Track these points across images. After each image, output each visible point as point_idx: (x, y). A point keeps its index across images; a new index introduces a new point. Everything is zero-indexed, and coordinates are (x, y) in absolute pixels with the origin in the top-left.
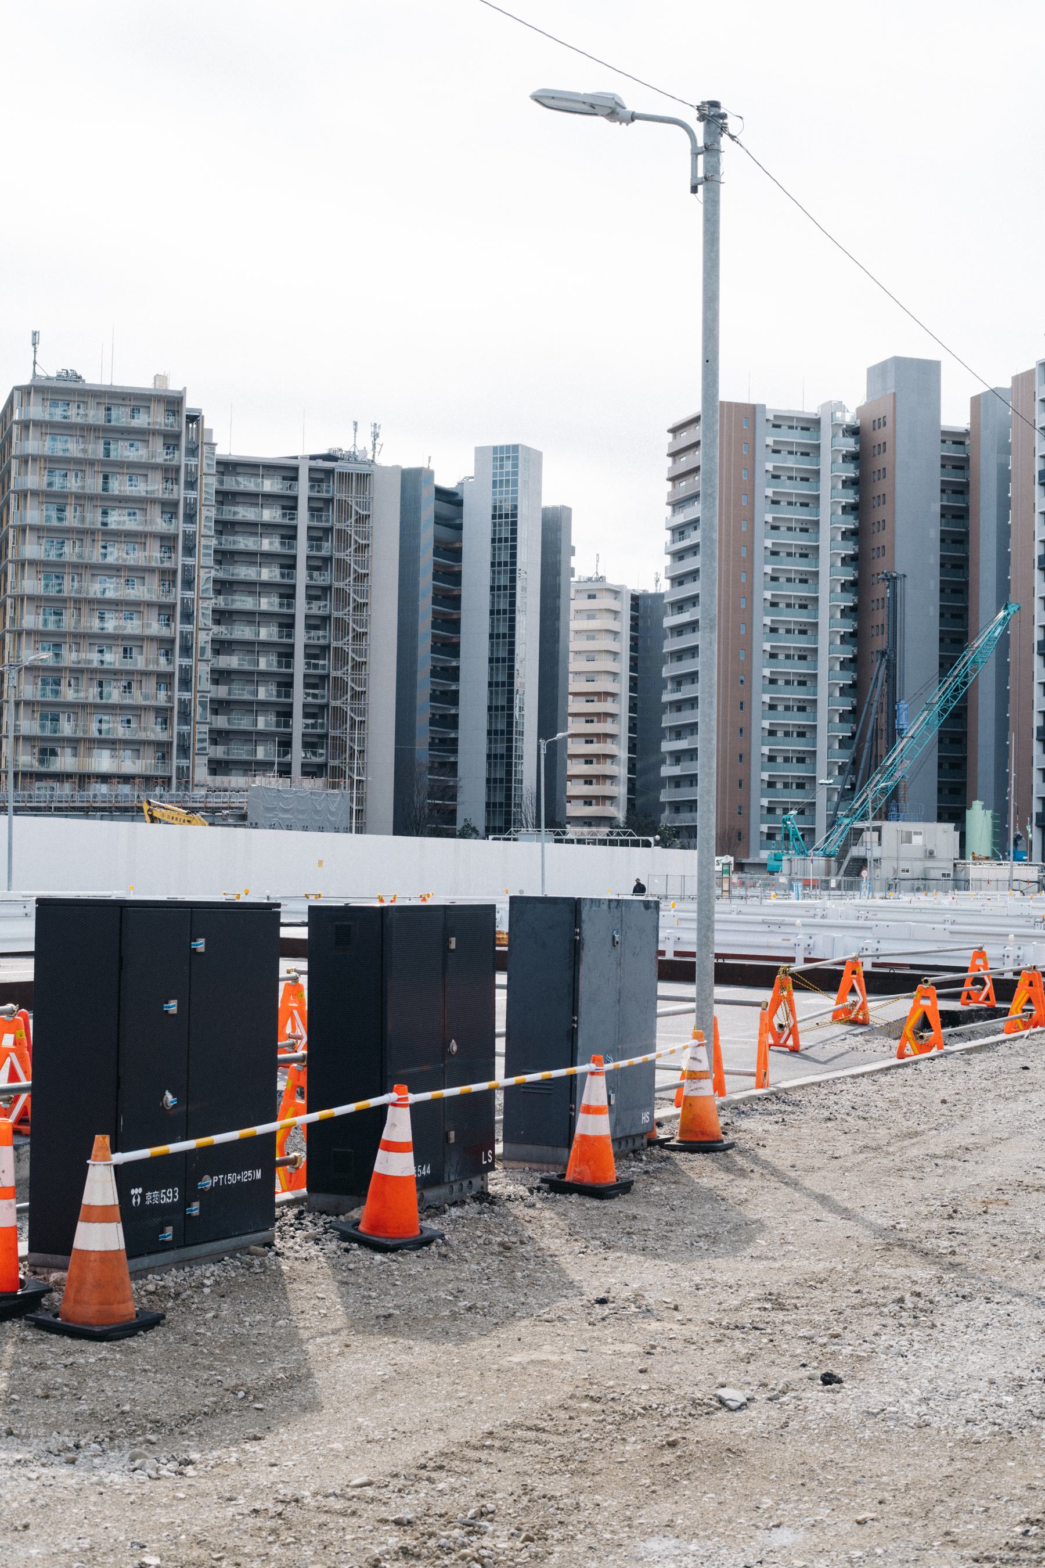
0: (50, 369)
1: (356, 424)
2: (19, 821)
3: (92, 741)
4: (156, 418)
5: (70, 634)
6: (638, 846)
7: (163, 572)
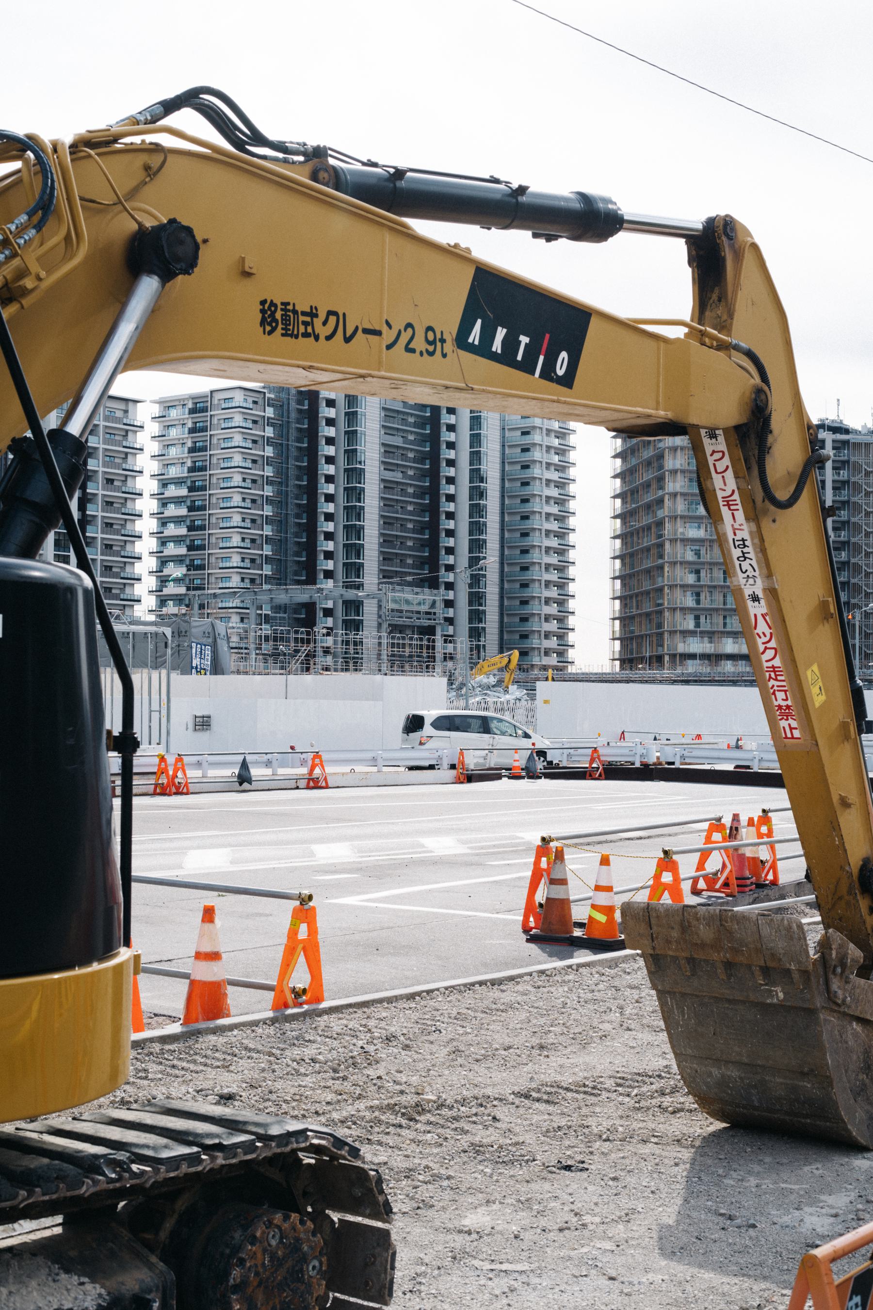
1: (838, 400)
5: (707, 563)
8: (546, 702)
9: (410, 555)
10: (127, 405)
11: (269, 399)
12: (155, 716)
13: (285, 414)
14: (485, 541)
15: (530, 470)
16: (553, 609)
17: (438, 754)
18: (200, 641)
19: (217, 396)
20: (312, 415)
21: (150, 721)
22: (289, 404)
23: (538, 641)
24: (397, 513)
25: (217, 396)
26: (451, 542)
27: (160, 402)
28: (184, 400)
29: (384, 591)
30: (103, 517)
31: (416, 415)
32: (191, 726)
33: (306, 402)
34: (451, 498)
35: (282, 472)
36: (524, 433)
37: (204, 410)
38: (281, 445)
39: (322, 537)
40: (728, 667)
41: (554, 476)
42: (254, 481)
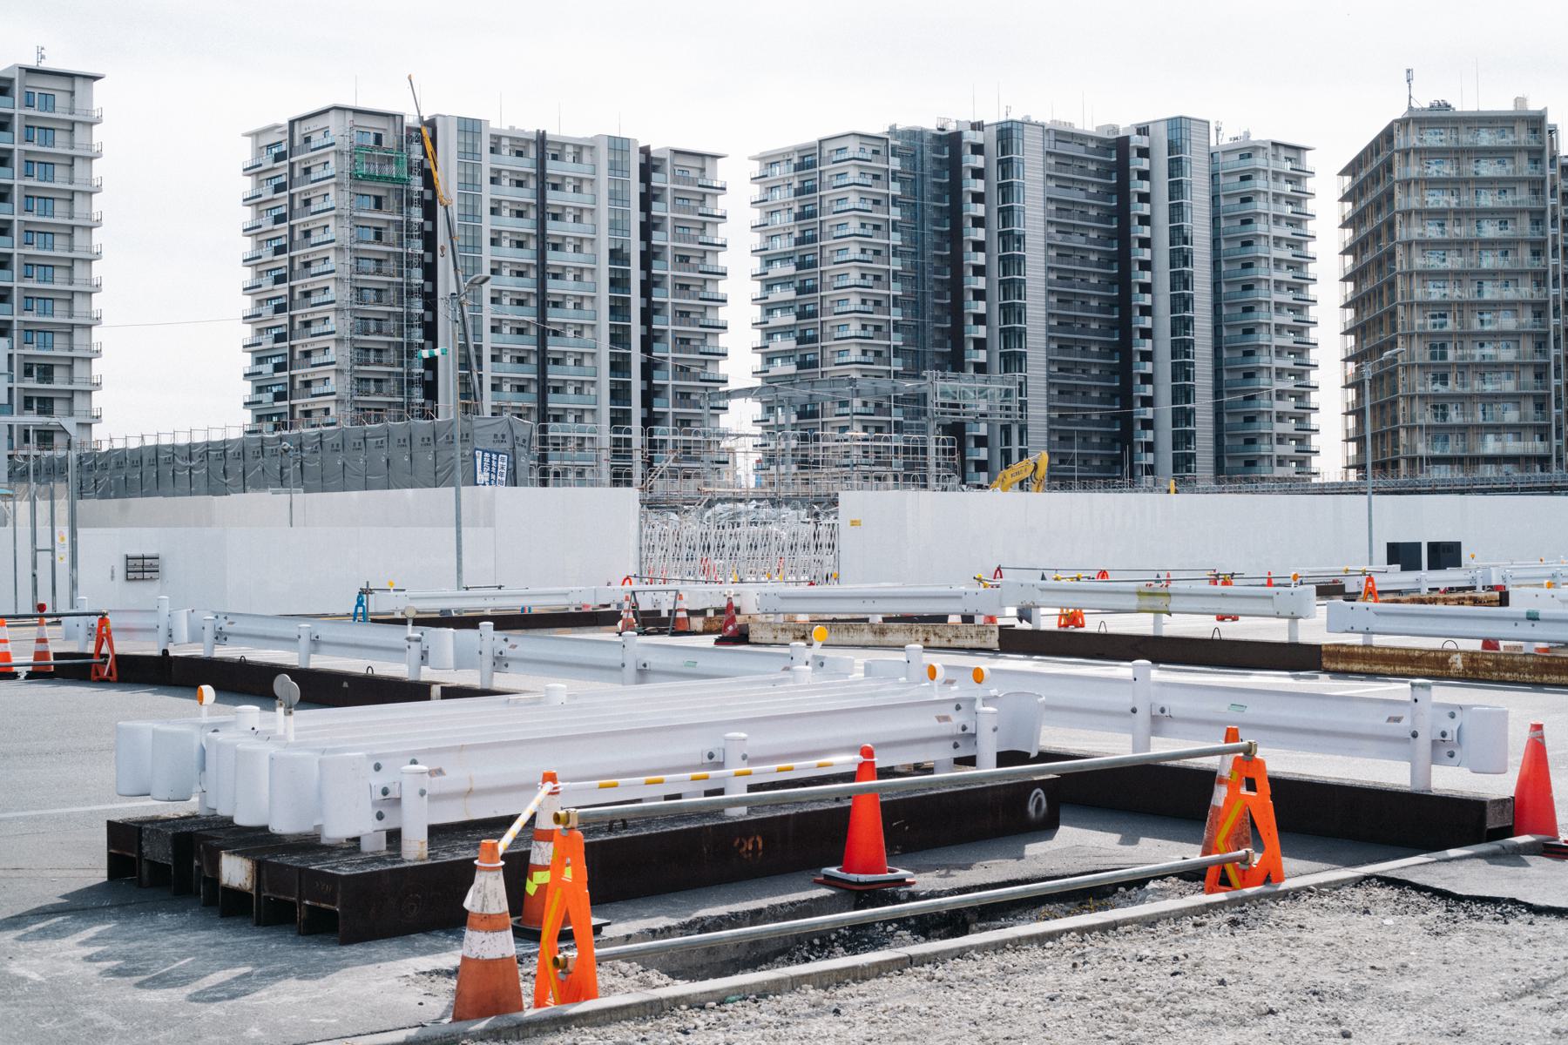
0: (1423, 101)
2: (1374, 497)
3: (1479, 427)
4: (1523, 137)
6: (1434, 547)
7: (1535, 273)
8: (854, 523)
9: (1095, 341)
10: (73, 83)
11: (894, 148)
12: (44, 559)
13: (919, 166)
14: (1191, 319)
15: (1253, 225)
16: (1289, 405)
17: (1473, 574)
18: (490, 446)
19: (828, 147)
20: (955, 165)
21: (35, 566)
22: (922, 153)
23: (1269, 447)
24: (1074, 287)
25: (828, 147)
26: (1147, 322)
27: (760, 159)
28: (788, 153)
29: (929, 378)
30: (675, 304)
31: (1098, 162)
32: (120, 572)
33: (947, 150)
34: (1146, 266)
35: (916, 239)
36: (1243, 179)
37: (812, 165)
38: (914, 205)
39: (971, 321)
40: (1489, 471)
41: (1285, 231)
42: (877, 253)
